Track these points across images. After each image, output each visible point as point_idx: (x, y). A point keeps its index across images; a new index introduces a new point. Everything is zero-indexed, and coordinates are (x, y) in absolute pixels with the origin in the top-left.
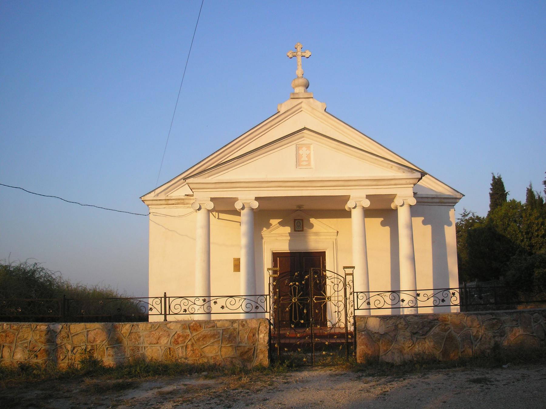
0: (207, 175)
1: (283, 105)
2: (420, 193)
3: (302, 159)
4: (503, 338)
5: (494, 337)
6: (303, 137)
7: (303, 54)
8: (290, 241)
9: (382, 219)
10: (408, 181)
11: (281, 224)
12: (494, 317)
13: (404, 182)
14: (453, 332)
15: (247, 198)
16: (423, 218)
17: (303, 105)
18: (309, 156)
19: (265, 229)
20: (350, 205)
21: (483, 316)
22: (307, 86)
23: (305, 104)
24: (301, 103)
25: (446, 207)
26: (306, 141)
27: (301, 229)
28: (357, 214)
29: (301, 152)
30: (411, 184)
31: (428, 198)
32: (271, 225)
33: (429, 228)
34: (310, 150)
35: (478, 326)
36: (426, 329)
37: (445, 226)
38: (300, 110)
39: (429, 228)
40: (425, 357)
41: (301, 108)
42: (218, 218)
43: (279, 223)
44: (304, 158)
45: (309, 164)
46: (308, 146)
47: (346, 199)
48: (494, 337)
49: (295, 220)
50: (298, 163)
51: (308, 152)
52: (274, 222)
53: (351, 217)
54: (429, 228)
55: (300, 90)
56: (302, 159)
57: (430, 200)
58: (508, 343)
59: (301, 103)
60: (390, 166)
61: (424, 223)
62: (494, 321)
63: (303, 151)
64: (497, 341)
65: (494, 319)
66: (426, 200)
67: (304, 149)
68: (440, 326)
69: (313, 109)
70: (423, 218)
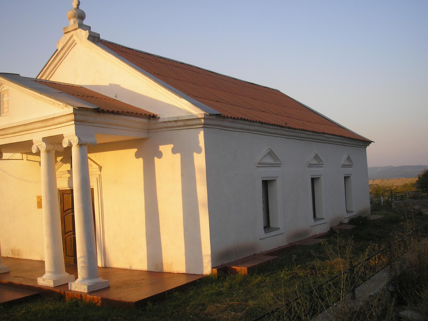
9: (136, 150)
17: (75, 38)
24: (72, 36)
30: (71, 121)
33: (178, 156)
37: (195, 154)
38: (74, 44)
39: (178, 156)
42: (27, 160)
43: (60, 161)
57: (174, 124)
59: (72, 36)
60: (53, 103)
61: (174, 151)
66: (170, 125)
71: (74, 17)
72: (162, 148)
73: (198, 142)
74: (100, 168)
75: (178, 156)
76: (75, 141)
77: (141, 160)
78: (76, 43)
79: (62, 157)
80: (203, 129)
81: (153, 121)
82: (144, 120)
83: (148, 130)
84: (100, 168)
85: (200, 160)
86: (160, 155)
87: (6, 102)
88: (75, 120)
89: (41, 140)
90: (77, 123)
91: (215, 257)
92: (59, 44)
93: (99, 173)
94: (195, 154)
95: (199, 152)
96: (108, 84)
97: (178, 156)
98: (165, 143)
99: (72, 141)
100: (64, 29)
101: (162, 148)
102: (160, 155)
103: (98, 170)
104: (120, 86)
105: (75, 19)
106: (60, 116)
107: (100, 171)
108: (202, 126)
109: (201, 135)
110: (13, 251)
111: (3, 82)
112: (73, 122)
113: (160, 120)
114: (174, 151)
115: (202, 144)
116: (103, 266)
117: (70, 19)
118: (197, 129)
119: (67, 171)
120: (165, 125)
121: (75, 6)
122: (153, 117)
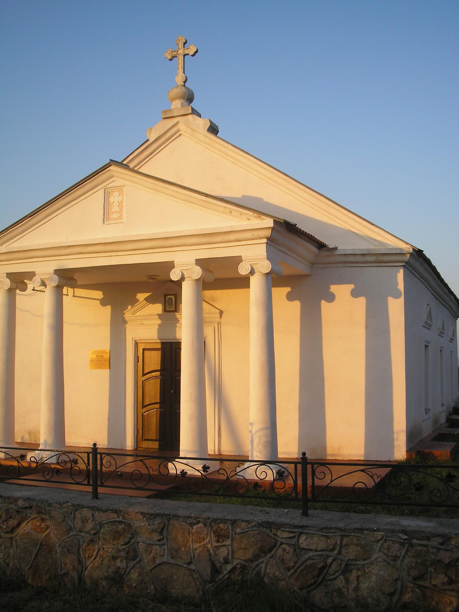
1: (153, 131)
2: (325, 248)
3: (113, 210)
5: (114, 558)
6: (112, 177)
8: (159, 325)
9: (288, 289)
10: (256, 234)
11: (149, 300)
12: (120, 519)
14: (52, 536)
16: (352, 286)
17: (181, 126)
18: (120, 204)
19: (130, 307)
20: (243, 270)
21: (101, 514)
22: (190, 99)
24: (178, 123)
25: (390, 268)
26: (117, 182)
27: (173, 309)
28: (256, 282)
29: (111, 199)
30: (261, 238)
31: (355, 255)
32: (138, 301)
34: (123, 196)
35: (93, 532)
36: (13, 522)
37: (390, 299)
41: (179, 131)
42: (74, 296)
44: (115, 208)
46: (120, 189)
47: (170, 265)
48: (114, 558)
49: (165, 296)
51: (121, 198)
52: (141, 297)
53: (249, 288)
55: (177, 104)
56: (113, 210)
57: (359, 259)
59: (178, 123)
60: (228, 211)
61: (355, 294)
62: (121, 527)
63: (114, 198)
65: (120, 522)
66: (353, 259)
67: (116, 194)
69: (193, 130)
70: (352, 286)
72: (334, 288)
73: (397, 284)
74: (221, 313)
75: (362, 301)
77: (297, 304)
78: (181, 135)
81: (324, 253)
82: (314, 249)
83: (312, 264)
84: (221, 313)
85: (396, 309)
86: (331, 298)
88: (269, 239)
89: (194, 262)
90: (270, 243)
91: (412, 435)
92: (150, 133)
93: (218, 320)
94: (390, 299)
95: (396, 296)
96: (240, 196)
97: (362, 301)
100: (165, 111)
101: (334, 288)
102: (331, 298)
103: (218, 315)
104: (261, 200)
105: (182, 101)
106: (244, 230)
108: (404, 264)
111: (115, 174)
112: (265, 241)
114: (355, 294)
115: (401, 286)
117: (173, 100)
118: (393, 268)
119: (158, 315)
120: (344, 259)
122: (321, 246)
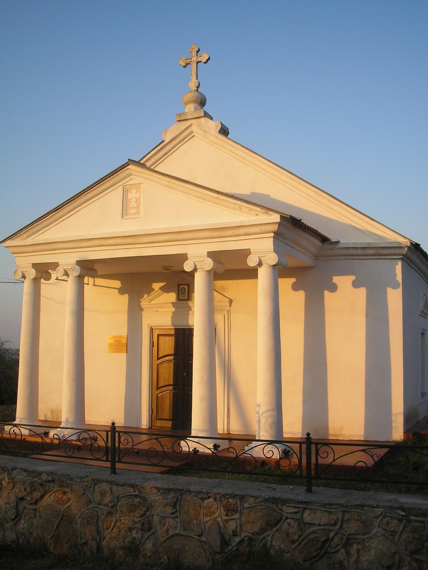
0: (25, 236)
4: (147, 535)
6: (131, 175)
7: (199, 59)
9: (294, 280)
10: (264, 228)
12: (137, 493)
13: (257, 229)
14: (73, 507)
15: (68, 260)
16: (353, 277)
18: (138, 200)
19: (146, 296)
20: (252, 262)
22: (202, 103)
23: (195, 126)
24: (191, 125)
26: (135, 180)
28: (264, 274)
29: (130, 196)
30: (268, 232)
31: (356, 248)
32: (153, 290)
33: (362, 292)
34: (140, 193)
35: (110, 505)
36: (37, 495)
37: (389, 290)
38: (191, 136)
39: (362, 292)
40: (32, 540)
41: (192, 132)
42: (94, 285)
43: (161, 288)
44: (133, 204)
45: (138, 213)
46: (137, 186)
47: (184, 257)
49: (179, 285)
50: (124, 213)
52: (157, 286)
54: (362, 293)
55: (190, 108)
57: (360, 252)
58: (154, 545)
59: (191, 125)
60: (238, 207)
61: (356, 285)
62: (137, 500)
63: (132, 195)
64: (134, 538)
65: (136, 496)
66: (354, 252)
67: (134, 191)
68: (57, 494)
69: (205, 132)
70: (353, 277)
71: (195, 102)
72: (336, 279)
73: (395, 275)
74: (231, 301)
76: (272, 258)
78: (194, 136)
79: (165, 283)
80: (401, 260)
82: (318, 242)
83: (316, 257)
84: (231, 301)
85: (395, 299)
86: (333, 288)
87: (133, 201)
89: (206, 255)
92: (166, 134)
93: (228, 308)
94: (389, 290)
98: (343, 273)
99: (262, 259)
100: (179, 115)
101: (336, 279)
102: (333, 288)
103: (228, 304)
104: (269, 196)
107: (230, 305)
108: (402, 257)
109: (399, 267)
110: (52, 412)
111: (133, 172)
112: (272, 235)
113: (339, 246)
114: (356, 285)
116: (226, 432)
117: (186, 104)
121: (194, 88)
